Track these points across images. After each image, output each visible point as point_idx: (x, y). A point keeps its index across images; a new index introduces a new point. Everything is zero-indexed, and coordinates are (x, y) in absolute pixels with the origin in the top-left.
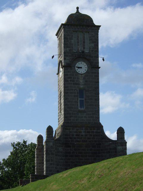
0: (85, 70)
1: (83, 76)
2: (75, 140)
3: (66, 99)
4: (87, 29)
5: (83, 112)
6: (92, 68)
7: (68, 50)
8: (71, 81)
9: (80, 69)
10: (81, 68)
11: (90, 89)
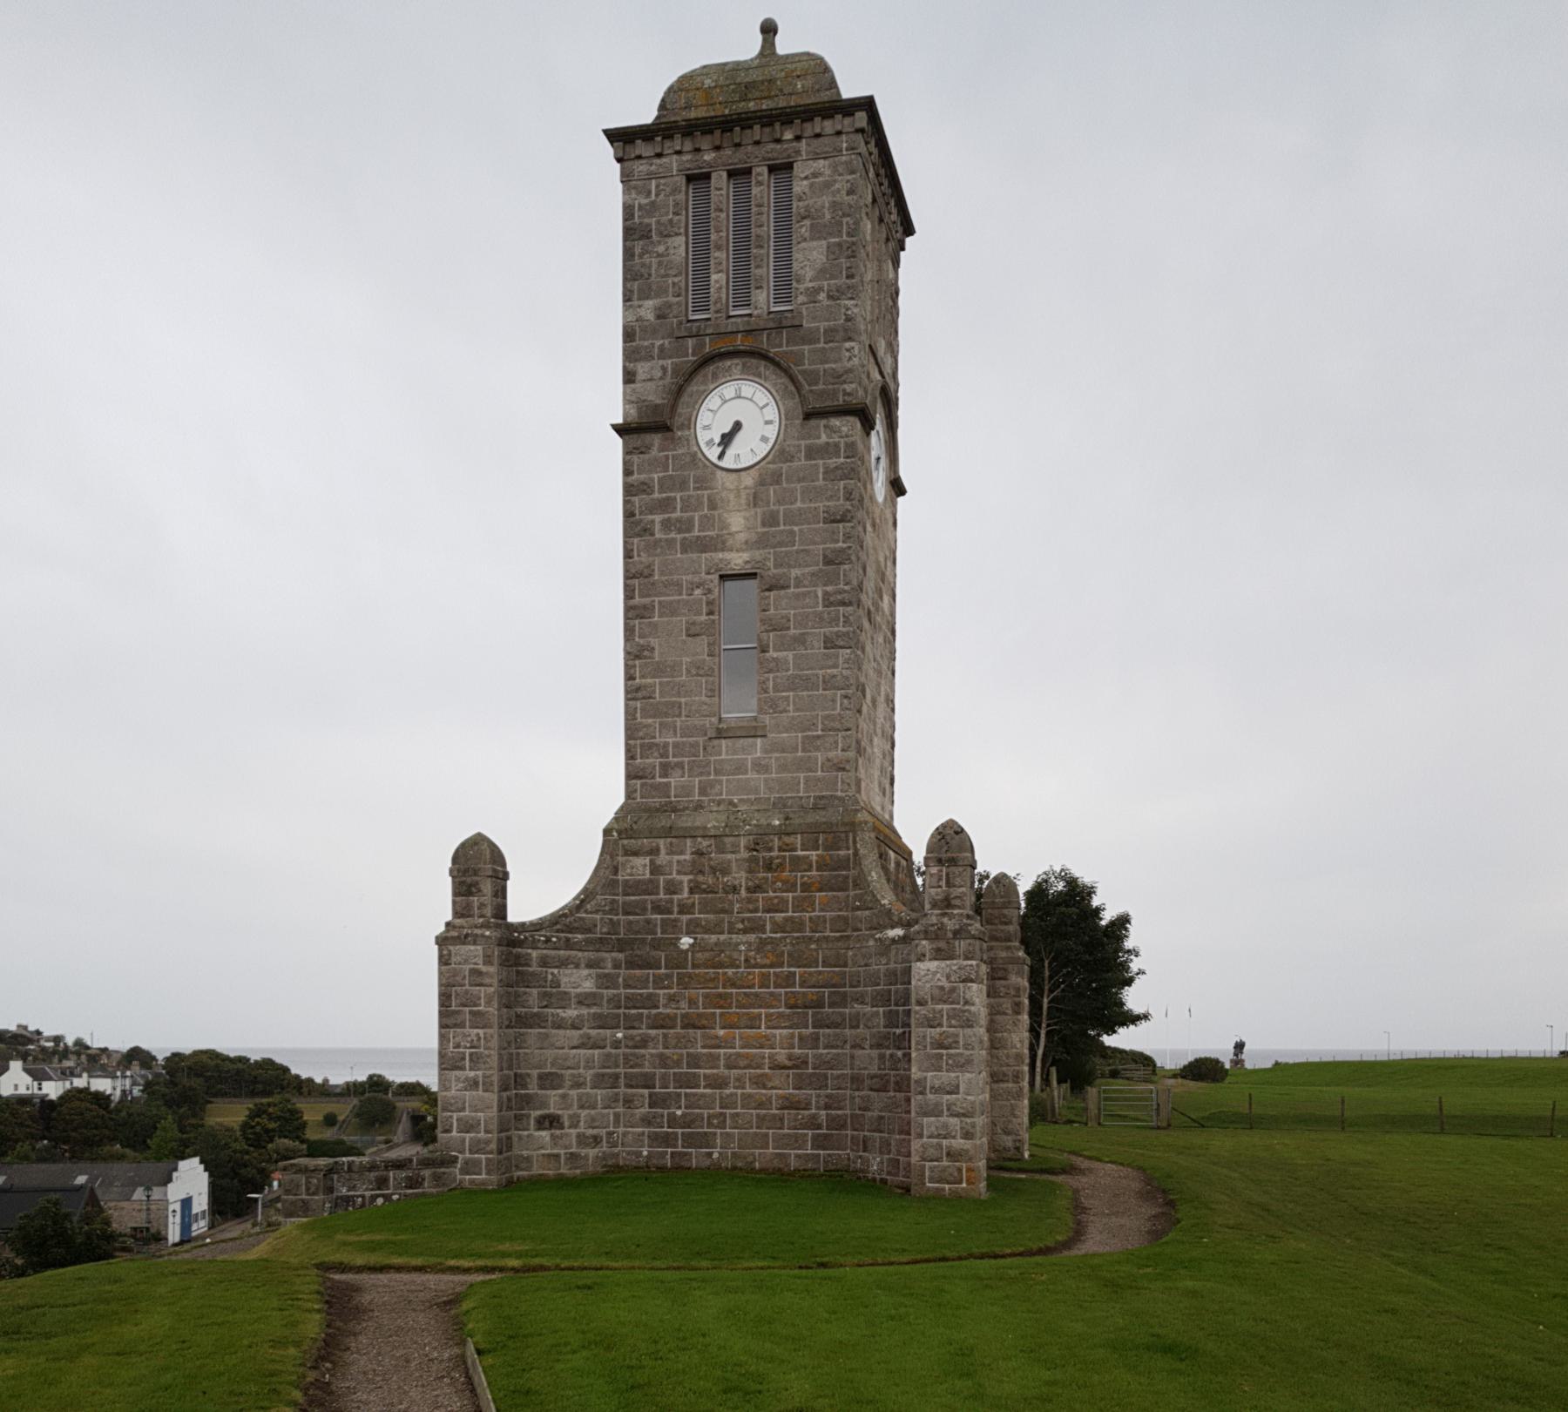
0: (764, 439)
1: (748, 480)
2: (685, 918)
3: (638, 657)
4: (778, 141)
5: (753, 731)
6: (808, 416)
7: (651, 316)
8: (667, 525)
9: (739, 438)
10: (737, 426)
11: (795, 572)
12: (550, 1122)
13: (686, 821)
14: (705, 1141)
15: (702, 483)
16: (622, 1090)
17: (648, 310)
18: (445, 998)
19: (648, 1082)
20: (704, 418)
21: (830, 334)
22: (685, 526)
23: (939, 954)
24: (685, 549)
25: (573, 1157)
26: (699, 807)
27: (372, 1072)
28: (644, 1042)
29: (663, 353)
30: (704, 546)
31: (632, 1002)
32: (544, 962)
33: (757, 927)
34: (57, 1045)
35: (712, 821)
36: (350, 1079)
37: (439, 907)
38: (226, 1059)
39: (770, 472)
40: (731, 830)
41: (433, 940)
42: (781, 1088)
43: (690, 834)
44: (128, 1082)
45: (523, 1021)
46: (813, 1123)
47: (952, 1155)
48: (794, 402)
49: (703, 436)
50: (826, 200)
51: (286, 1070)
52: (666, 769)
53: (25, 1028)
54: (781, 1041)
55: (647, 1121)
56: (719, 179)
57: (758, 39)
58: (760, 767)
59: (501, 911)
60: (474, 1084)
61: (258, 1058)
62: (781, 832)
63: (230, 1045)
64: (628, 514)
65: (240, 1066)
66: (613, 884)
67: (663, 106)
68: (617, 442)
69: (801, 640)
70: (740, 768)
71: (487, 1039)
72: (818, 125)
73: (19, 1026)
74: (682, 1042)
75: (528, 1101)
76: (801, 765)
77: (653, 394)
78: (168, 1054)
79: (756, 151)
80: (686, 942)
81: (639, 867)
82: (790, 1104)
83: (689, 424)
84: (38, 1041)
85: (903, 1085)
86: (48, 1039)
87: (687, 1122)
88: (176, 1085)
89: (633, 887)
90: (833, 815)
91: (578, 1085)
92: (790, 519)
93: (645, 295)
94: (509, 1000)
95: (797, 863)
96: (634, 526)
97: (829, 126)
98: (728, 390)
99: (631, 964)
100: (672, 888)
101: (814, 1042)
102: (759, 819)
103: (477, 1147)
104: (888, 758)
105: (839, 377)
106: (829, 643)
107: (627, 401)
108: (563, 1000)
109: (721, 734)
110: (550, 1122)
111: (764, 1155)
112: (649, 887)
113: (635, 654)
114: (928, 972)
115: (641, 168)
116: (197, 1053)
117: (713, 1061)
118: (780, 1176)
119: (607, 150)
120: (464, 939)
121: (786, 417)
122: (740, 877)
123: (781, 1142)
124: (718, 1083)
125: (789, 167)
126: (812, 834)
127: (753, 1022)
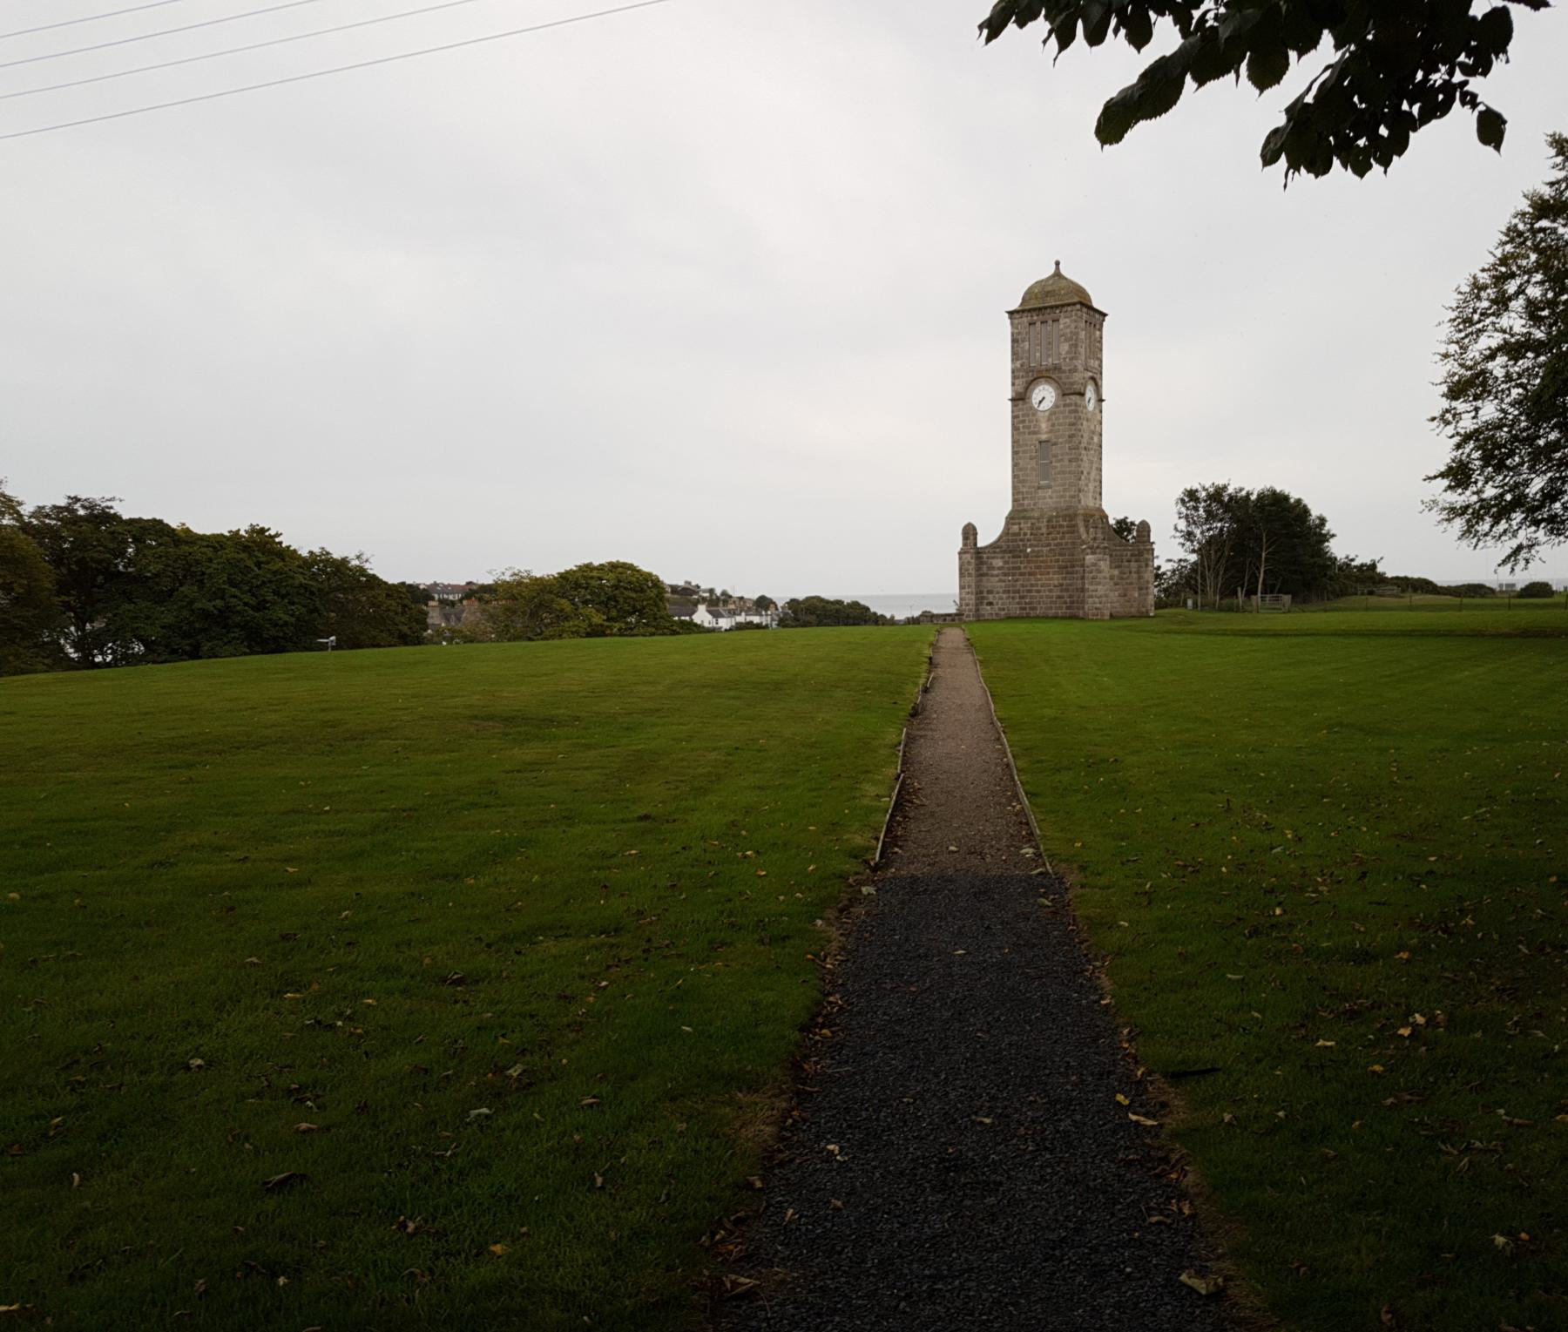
1: (1047, 414)
6: (1064, 395)
11: (1060, 440)
12: (990, 604)
13: (1029, 514)
14: (1035, 609)
15: (1034, 415)
16: (1011, 595)
17: (1018, 364)
18: (960, 569)
19: (1018, 592)
20: (1034, 396)
21: (1070, 370)
22: (1029, 427)
23: (1093, 553)
24: (1029, 433)
25: (997, 614)
26: (1033, 510)
27: (924, 609)
28: (1017, 580)
29: (1023, 377)
30: (1034, 433)
31: (1014, 568)
32: (988, 558)
33: (1049, 545)
34: (711, 595)
35: (1036, 514)
36: (910, 615)
37: (959, 544)
38: (828, 602)
39: (1053, 412)
40: (1042, 516)
41: (966, 523)
42: (1056, 593)
43: (1030, 518)
44: (769, 618)
45: (982, 575)
46: (1065, 603)
47: (1096, 609)
48: (1059, 391)
49: (1034, 401)
50: (1068, 331)
51: (867, 609)
52: (1023, 499)
53: (690, 583)
54: (1056, 579)
55: (1018, 603)
56: (1038, 324)
57: (1054, 267)
58: (1051, 497)
59: (975, 544)
60: (968, 593)
61: (849, 601)
62: (1056, 517)
63: (829, 594)
64: (1013, 424)
65: (838, 606)
66: (1008, 534)
67: (1024, 299)
68: (1010, 403)
69: (1062, 460)
70: (1045, 498)
71: (971, 580)
72: (1065, 309)
73: (686, 582)
74: (1028, 580)
75: (983, 598)
76: (1062, 496)
77: (1020, 389)
78: (788, 600)
79: (1049, 317)
80: (1029, 550)
81: (1015, 528)
82: (1059, 597)
83: (1030, 398)
84: (698, 592)
85: (1083, 590)
86: (704, 591)
87: (1030, 603)
88: (798, 620)
89: (1014, 534)
90: (1071, 512)
91: (998, 593)
92: (1059, 424)
93: (1017, 360)
94: (978, 569)
95: (1061, 526)
96: (1015, 428)
97: (1069, 309)
98: (1041, 388)
99: (1013, 557)
100: (1025, 534)
101: (1065, 579)
102: (1050, 513)
103: (970, 610)
104: (1098, 490)
105: (1072, 384)
106: (1070, 461)
107: (1013, 391)
108: (994, 568)
109: (1039, 488)
110: (990, 604)
111: (1052, 612)
112: (1019, 534)
113: (1015, 465)
114: (1090, 558)
115: (1016, 321)
116: (808, 599)
117: (1037, 585)
118: (1055, 617)
119: (1007, 315)
120: (965, 553)
121: (1057, 395)
122: (1044, 530)
123: (1057, 608)
124: (1039, 591)
125: (1058, 320)
126: (1064, 517)
127: (1048, 573)
